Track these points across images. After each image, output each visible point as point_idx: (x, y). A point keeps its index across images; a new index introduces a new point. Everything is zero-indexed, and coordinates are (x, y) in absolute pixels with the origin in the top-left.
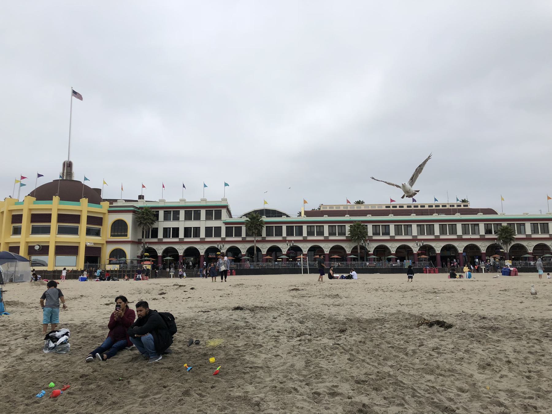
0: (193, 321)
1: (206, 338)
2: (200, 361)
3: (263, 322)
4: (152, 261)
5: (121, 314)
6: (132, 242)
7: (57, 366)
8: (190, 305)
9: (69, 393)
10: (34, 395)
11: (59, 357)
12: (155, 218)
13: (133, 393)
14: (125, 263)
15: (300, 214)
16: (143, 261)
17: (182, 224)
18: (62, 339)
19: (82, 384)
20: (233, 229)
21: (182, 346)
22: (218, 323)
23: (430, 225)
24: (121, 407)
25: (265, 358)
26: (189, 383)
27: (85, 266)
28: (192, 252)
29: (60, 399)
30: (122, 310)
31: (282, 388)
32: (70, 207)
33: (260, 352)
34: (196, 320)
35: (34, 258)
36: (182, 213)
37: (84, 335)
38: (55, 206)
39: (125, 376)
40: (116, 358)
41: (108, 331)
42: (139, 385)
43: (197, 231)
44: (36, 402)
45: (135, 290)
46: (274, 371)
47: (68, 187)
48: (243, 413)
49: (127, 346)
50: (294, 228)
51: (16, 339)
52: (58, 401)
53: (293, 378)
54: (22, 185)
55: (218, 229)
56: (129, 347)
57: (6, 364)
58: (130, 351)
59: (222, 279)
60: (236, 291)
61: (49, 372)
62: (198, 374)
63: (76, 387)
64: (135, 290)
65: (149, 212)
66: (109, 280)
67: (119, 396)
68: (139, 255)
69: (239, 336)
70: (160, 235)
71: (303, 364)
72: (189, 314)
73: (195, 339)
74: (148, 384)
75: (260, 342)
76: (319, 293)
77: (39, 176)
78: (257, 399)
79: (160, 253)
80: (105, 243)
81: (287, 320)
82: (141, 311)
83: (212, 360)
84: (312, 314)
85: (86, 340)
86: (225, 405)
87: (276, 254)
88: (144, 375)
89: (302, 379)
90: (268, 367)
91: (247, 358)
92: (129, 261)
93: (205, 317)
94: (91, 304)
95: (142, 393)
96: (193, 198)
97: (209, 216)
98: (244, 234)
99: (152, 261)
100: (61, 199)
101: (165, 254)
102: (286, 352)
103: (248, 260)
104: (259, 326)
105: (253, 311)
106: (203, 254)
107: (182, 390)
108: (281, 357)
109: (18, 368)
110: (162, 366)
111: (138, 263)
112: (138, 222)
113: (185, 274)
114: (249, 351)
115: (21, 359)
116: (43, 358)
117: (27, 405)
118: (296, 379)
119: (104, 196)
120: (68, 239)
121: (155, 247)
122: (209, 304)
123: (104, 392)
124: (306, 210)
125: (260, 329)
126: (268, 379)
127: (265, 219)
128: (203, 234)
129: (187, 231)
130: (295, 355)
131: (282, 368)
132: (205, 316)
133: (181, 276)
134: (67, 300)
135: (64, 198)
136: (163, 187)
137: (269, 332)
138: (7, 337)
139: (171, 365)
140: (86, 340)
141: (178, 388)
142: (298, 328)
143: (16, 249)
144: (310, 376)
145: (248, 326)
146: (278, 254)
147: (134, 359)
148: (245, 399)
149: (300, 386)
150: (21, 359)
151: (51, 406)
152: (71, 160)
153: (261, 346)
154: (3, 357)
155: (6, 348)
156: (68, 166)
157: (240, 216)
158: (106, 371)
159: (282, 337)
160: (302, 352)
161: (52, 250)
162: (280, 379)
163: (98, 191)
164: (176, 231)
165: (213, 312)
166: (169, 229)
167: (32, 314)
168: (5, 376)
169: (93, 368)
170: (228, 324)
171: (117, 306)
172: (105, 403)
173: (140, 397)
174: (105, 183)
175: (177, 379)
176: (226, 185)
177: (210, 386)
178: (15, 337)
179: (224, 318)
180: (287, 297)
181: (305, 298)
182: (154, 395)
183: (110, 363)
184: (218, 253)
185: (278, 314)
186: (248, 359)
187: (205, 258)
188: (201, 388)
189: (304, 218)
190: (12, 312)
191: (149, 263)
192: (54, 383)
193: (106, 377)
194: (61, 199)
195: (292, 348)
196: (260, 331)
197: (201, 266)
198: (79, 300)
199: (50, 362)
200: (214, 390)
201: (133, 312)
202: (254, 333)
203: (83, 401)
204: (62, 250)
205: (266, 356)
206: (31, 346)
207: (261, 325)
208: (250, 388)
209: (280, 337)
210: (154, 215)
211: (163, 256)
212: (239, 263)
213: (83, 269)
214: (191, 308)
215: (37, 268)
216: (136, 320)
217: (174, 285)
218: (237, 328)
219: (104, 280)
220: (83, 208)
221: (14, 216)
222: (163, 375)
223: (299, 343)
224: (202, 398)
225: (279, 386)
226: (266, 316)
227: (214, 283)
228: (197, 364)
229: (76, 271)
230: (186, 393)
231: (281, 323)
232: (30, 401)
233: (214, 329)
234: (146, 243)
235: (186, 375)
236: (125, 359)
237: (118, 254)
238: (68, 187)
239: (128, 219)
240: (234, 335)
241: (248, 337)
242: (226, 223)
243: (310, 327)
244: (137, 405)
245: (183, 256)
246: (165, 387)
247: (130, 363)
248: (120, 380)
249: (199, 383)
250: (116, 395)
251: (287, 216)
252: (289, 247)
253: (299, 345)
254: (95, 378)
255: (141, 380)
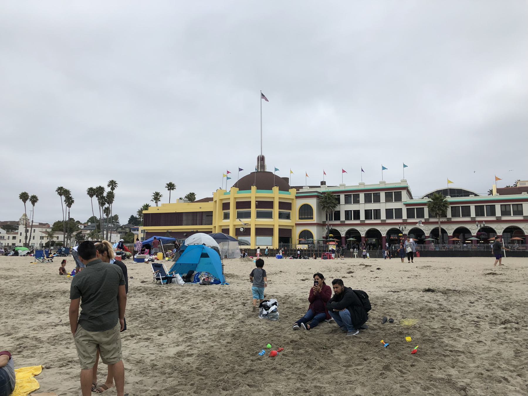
0: (384, 300)
1: (399, 317)
2: (396, 339)
3: (459, 306)
4: (337, 242)
5: (319, 289)
6: (317, 224)
7: (271, 330)
8: (378, 284)
9: (283, 355)
10: (256, 353)
11: (272, 323)
12: (337, 202)
13: (337, 362)
14: (313, 243)
15: (491, 192)
16: (328, 241)
17: (362, 207)
18: (273, 308)
19: (293, 348)
20: (415, 211)
21: (376, 323)
22: (410, 303)
23: (517, 205)
24: (328, 373)
25: (466, 343)
26: (387, 358)
27: (280, 246)
28: (373, 233)
29: (277, 358)
30: (320, 286)
31: (489, 376)
32: (265, 195)
33: (459, 336)
34: (387, 299)
35: (240, 238)
36: (362, 196)
37: (288, 306)
38: (253, 195)
39: (327, 345)
40: (318, 328)
41: (308, 304)
42: (342, 355)
43: (377, 213)
44: (259, 359)
45: (336, 269)
46: (477, 357)
47: (262, 178)
48: (449, 395)
49: (326, 319)
50: (485, 208)
51: (237, 306)
52: (276, 360)
53: (502, 367)
54: (228, 178)
55: (399, 212)
56: (328, 319)
57: (232, 326)
58: (329, 324)
59: (409, 260)
60: (423, 273)
61: (265, 335)
62: (395, 351)
63: (289, 350)
64: (336, 269)
65: (331, 196)
66: (301, 258)
67: (325, 362)
68: (325, 236)
69: (433, 318)
70: (343, 217)
71: (512, 353)
72: (379, 293)
73: (388, 318)
74: (349, 355)
75: (459, 326)
76: (523, 279)
77: (240, 170)
78: (462, 384)
79: (343, 234)
80: (294, 225)
81: (486, 306)
82: (337, 288)
83: (408, 339)
84: (516, 301)
85: (290, 310)
86: (428, 385)
87: (464, 236)
88: (345, 346)
89: (512, 369)
90: (470, 353)
91: (446, 340)
92: (315, 242)
93: (396, 297)
94: (292, 279)
95: (345, 363)
96: (372, 181)
97: (389, 198)
98: (426, 216)
99: (337, 242)
100: (257, 189)
101: (348, 236)
102: (490, 339)
103: (433, 241)
104: (455, 310)
105: (446, 294)
106: (385, 235)
107: (382, 364)
108: (487, 345)
109: (242, 329)
110: (360, 340)
111: (324, 243)
112: (322, 206)
113: (368, 255)
114: (446, 334)
115: (242, 322)
116: (259, 323)
117: (252, 361)
118: (505, 369)
119: (291, 184)
120: (264, 222)
121: (338, 229)
122: (397, 284)
123: (312, 358)
124: (498, 187)
125: (456, 312)
126: (472, 365)
127: (449, 199)
128: (383, 216)
129: (368, 214)
130: (501, 344)
131: (487, 355)
132: (396, 296)
133: (365, 257)
134: (269, 274)
135: (261, 187)
136: (325, 173)
137: (467, 316)
138: (230, 303)
139: (368, 340)
140: (290, 310)
141: (378, 362)
142: (502, 315)
143: (226, 231)
144: (522, 367)
145: (441, 308)
146: (467, 235)
147: (334, 331)
148: (449, 382)
149: (511, 377)
150: (242, 322)
151: (271, 364)
152: (263, 154)
153: (460, 330)
154: (229, 319)
155: (231, 313)
156: (261, 159)
157: (421, 197)
158: (311, 339)
159: (483, 323)
160: (509, 341)
161: (253, 232)
162: (485, 367)
163: (286, 180)
164: (357, 214)
165: (403, 292)
166: (350, 212)
167: (246, 285)
168: (233, 335)
169: (300, 336)
170: (421, 305)
171: (315, 282)
172: (314, 367)
173: (344, 366)
174: (291, 172)
175: (376, 354)
176: (405, 166)
177: (409, 364)
178: (236, 303)
179: (415, 299)
180: (483, 282)
181: (505, 283)
182: (356, 366)
183: (313, 333)
184: (400, 235)
185: (475, 299)
186: (447, 342)
187: (386, 240)
188: (400, 365)
189: (496, 196)
190: (231, 283)
191: (334, 243)
192: (271, 344)
193: (312, 345)
194: (257, 189)
195: (497, 335)
196: (456, 315)
197: (383, 246)
198: (279, 275)
199: (265, 327)
200: (413, 369)
201: (329, 288)
202: (450, 316)
203: (296, 363)
204: (262, 232)
205: (467, 341)
206: (249, 312)
207: (456, 309)
208: (453, 372)
209: (481, 323)
210: (336, 199)
211: (346, 237)
212: (422, 245)
213: (278, 248)
214: (380, 287)
215: (243, 247)
216: (332, 296)
217: (360, 265)
218: (430, 310)
219: (297, 258)
220: (275, 195)
221: (223, 204)
222: (362, 349)
223: (505, 331)
224: (404, 375)
225: (486, 374)
226: (461, 300)
227: (411, 263)
228: (393, 341)
229: (272, 250)
230: (387, 368)
231: (480, 308)
232: (254, 358)
233: (407, 309)
234: (330, 225)
235: (384, 350)
236: (326, 330)
237: (306, 235)
238: (262, 178)
239: (313, 203)
240: (428, 317)
241: (444, 320)
242: (407, 205)
243: (516, 314)
244: (342, 373)
245: (365, 237)
246: (365, 360)
247: (331, 335)
248: (324, 349)
249: (398, 360)
250: (323, 361)
251: (476, 195)
252: (479, 228)
253: (505, 333)
254: (303, 345)
255: (343, 350)
